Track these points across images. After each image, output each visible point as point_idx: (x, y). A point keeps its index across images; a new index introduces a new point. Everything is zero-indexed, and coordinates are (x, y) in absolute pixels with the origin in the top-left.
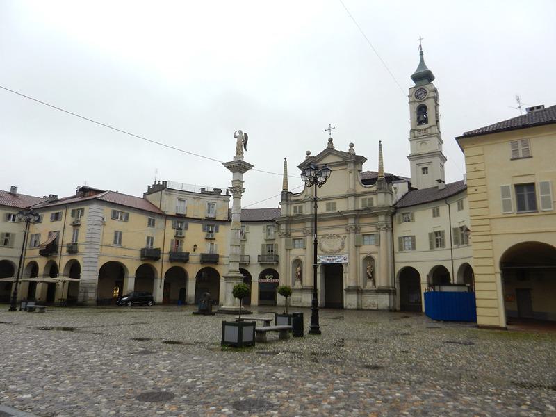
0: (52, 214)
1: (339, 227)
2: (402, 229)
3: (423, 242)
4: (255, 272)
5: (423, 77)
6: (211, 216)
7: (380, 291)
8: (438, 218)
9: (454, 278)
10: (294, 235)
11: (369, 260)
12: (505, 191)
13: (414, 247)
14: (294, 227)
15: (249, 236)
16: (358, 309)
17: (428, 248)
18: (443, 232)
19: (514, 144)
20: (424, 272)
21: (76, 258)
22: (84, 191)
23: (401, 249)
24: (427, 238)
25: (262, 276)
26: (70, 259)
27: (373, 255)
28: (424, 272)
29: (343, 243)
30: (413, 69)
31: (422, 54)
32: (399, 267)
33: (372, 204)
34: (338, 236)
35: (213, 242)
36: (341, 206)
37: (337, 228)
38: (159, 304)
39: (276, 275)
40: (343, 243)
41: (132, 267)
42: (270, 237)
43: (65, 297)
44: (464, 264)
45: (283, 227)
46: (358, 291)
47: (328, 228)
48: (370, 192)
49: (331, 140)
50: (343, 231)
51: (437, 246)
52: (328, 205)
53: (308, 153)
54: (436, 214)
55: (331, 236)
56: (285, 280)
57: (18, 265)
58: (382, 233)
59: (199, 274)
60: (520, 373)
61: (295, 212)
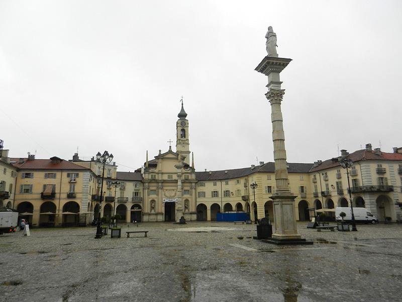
0: (23, 174)
2: (200, 189)
4: (129, 206)
5: (182, 115)
6: (109, 176)
7: (191, 213)
9: (234, 208)
10: (152, 188)
11: (187, 201)
12: (266, 187)
13: (205, 197)
16: (156, 222)
19: (268, 176)
21: (75, 201)
23: (199, 197)
24: (211, 193)
25: (133, 208)
26: (43, 202)
30: (179, 111)
31: (182, 104)
32: (198, 204)
33: (188, 178)
38: (129, 223)
39: (140, 207)
41: (37, 205)
42: (136, 189)
43: (61, 222)
44: (227, 204)
45: (147, 184)
46: (149, 214)
47: (169, 186)
48: (188, 173)
49: (170, 147)
53: (160, 151)
54: (215, 185)
55: (170, 190)
56: (147, 208)
57: (113, 206)
58: (193, 190)
60: (87, 266)
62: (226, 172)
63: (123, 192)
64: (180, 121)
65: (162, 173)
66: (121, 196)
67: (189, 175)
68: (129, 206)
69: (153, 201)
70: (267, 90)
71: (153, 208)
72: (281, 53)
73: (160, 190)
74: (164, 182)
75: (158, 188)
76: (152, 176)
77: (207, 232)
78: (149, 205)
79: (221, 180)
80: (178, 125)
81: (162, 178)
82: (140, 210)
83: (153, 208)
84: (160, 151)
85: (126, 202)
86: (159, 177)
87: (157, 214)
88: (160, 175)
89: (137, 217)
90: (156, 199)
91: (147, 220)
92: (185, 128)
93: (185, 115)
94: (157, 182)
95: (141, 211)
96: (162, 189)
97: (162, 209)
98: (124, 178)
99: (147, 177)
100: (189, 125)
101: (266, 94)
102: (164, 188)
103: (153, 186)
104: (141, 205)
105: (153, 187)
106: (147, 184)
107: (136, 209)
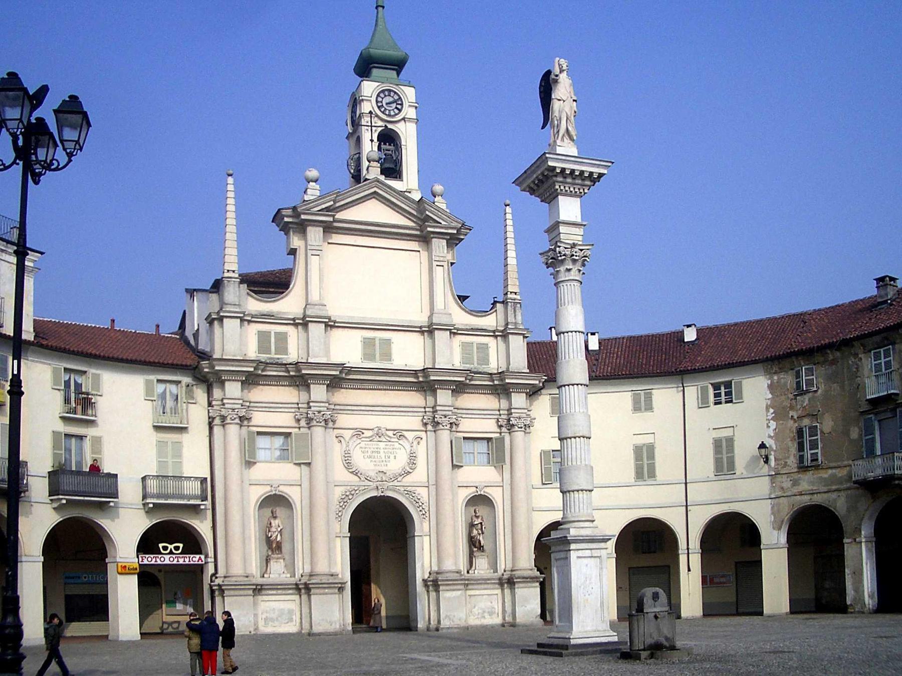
1: (885, 411)
8: (649, 414)
10: (260, 419)
14: (263, 394)
15: (104, 405)
17: (712, 476)
25: (147, 544)
29: (413, 458)
33: (485, 360)
34: (400, 434)
36: (409, 353)
39: (193, 544)
40: (413, 458)
45: (233, 389)
47: (371, 409)
50: (414, 422)
52: (368, 344)
54: (643, 405)
55: (379, 434)
61: (464, 360)
63: (178, 445)
65: (330, 325)
66: (161, 464)
71: (279, 547)
73: (318, 431)
74: (340, 378)
76: (263, 338)
77: (451, 442)
81: (327, 353)
82: (195, 559)
83: (273, 547)
87: (304, 589)
90: (294, 494)
94: (299, 377)
95: (199, 569)
103: (271, 407)
104: (203, 527)
105: (274, 406)
106: (233, 389)
107: (170, 556)
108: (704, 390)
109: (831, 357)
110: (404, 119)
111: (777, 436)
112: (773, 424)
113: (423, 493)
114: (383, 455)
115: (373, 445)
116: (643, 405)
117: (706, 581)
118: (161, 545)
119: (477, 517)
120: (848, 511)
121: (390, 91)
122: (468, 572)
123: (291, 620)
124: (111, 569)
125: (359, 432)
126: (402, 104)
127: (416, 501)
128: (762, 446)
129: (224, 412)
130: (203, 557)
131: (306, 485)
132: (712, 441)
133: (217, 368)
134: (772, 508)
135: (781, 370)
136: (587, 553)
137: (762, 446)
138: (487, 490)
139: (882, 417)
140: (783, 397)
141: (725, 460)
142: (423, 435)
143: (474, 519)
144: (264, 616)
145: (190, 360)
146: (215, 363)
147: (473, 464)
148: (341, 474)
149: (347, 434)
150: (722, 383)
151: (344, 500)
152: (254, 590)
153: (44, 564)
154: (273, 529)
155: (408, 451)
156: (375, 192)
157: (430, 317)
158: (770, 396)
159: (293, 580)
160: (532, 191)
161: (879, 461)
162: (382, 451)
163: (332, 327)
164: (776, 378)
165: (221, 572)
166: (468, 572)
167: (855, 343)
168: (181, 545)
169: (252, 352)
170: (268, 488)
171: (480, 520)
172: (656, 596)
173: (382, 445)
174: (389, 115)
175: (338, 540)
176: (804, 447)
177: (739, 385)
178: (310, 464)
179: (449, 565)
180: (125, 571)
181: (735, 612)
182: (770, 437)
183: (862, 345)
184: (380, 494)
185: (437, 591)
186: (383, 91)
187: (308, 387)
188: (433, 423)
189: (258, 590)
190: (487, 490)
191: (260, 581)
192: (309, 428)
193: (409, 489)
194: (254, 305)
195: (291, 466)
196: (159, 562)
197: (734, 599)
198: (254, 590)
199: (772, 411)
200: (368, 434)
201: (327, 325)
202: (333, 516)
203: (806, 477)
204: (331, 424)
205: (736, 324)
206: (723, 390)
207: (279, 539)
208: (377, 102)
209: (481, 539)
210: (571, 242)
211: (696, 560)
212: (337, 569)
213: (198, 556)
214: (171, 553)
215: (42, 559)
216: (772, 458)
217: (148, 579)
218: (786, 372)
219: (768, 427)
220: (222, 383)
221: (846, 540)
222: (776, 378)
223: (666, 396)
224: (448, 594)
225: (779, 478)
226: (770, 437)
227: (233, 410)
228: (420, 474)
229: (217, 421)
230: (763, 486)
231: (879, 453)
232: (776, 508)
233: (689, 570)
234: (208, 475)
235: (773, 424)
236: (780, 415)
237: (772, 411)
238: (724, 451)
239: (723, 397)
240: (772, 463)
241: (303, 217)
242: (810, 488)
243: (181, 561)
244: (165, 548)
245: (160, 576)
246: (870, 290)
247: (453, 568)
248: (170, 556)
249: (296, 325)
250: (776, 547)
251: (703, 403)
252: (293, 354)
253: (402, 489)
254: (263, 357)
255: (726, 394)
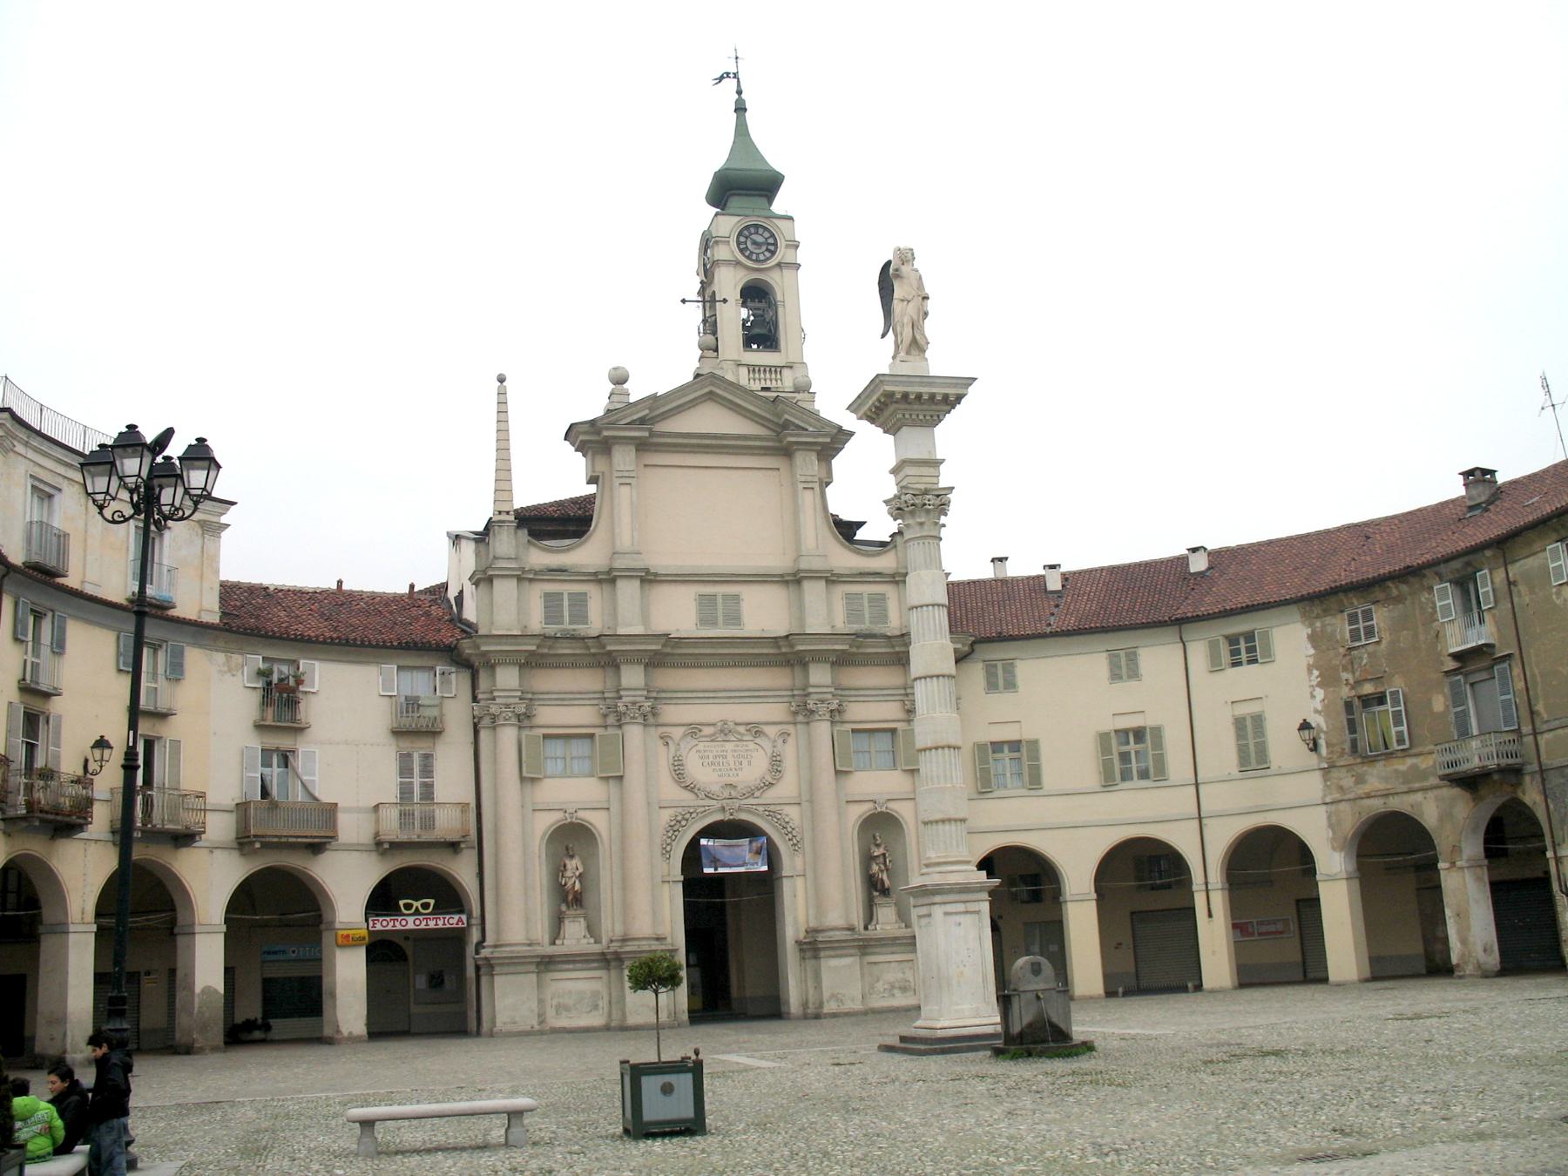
1: (1479, 670)
3: (1070, 760)
4: (347, 884)
5: (744, 187)
8: (1134, 684)
10: (549, 716)
13: (1035, 780)
16: (607, 1028)
17: (1235, 773)
18: (1157, 731)
20: (1205, 857)
22: (926, 314)
25: (382, 899)
27: (895, 807)
28: (1205, 857)
29: (776, 764)
30: (716, 156)
31: (740, 109)
33: (883, 617)
34: (756, 729)
35: (407, 722)
36: (764, 614)
37: (757, 701)
39: (448, 896)
45: (507, 678)
50: (772, 711)
51: (1126, 776)
52: (706, 602)
53: (619, 379)
55: (724, 731)
56: (516, 910)
59: (244, 900)
62: (1198, 564)
64: (729, 225)
65: (649, 578)
67: (889, 590)
68: (347, 884)
69: (572, 837)
70: (891, 490)
71: (577, 900)
72: (940, 362)
74: (664, 653)
75: (615, 715)
76: (552, 601)
78: (540, 875)
79: (1180, 623)
80: (721, 253)
81: (645, 618)
82: (453, 921)
83: (570, 899)
84: (619, 379)
85: (316, 848)
86: (629, 614)
88: (628, 590)
89: (430, 985)
91: (529, 1021)
92: (774, 279)
93: (766, 185)
94: (603, 655)
95: (456, 939)
96: (649, 718)
97: (660, 918)
98: (282, 630)
99: (507, 612)
100: (801, 256)
101: (886, 502)
102: (671, 713)
104: (462, 871)
105: (569, 700)
106: (507, 678)
107: (412, 919)
108: (1213, 646)
109: (1395, 592)
110: (779, 265)
111: (1326, 711)
112: (1320, 693)
113: (793, 813)
114: (730, 759)
115: (715, 748)
116: (1124, 669)
117: (1239, 927)
118: (401, 903)
119: (878, 846)
120: (1441, 819)
121: (757, 226)
122: (866, 928)
123: (596, 1007)
124: (327, 938)
125: (694, 730)
126: (775, 244)
127: (784, 826)
128: (1305, 726)
129: (493, 709)
130: (464, 917)
131: (615, 808)
132: (1231, 720)
133: (484, 648)
134: (1329, 818)
135: (1326, 612)
136: (961, 907)
137: (1305, 726)
138: (892, 805)
139: (1472, 679)
140: (1331, 653)
141: (1252, 748)
142: (791, 729)
143: (873, 848)
144: (554, 1002)
145: (447, 636)
146: (479, 641)
147: (869, 767)
148: (671, 792)
149: (677, 733)
150: (1242, 634)
151: (674, 828)
152: (538, 964)
153: (227, 936)
154: (568, 874)
155: (769, 751)
156: (711, 392)
157: (796, 560)
158: (1312, 651)
159: (597, 948)
160: (872, 420)
161: (1474, 744)
162: (729, 755)
163: (651, 581)
164: (1318, 624)
165: (489, 941)
166: (866, 928)
167: (1426, 572)
168: (432, 902)
169: (536, 623)
170: (560, 815)
171: (882, 850)
172: (1036, 969)
173: (729, 746)
174: (757, 261)
175: (666, 886)
176: (1359, 725)
177: (1266, 636)
178: (621, 778)
179: (834, 918)
180: (349, 942)
181: (1301, 977)
182: (1316, 711)
183: (1436, 573)
184: (727, 817)
185: (816, 957)
186: (747, 228)
187: (617, 667)
188: (803, 712)
189: (546, 963)
190: (892, 805)
191: (550, 950)
192: (620, 726)
193: (772, 808)
194: (539, 557)
195: (593, 781)
196: (399, 927)
197: (1298, 957)
198: (538, 964)
199: (1316, 673)
200: (707, 731)
201: (643, 581)
202: (658, 850)
203: (1375, 771)
204: (651, 720)
205: (1270, 543)
206: (1243, 646)
207: (577, 887)
208: (738, 243)
209: (885, 877)
210: (922, 487)
211: (1219, 900)
212: (664, 930)
213: (456, 917)
214: (417, 912)
215: (224, 928)
216: (1322, 742)
217: (382, 952)
218: (1333, 615)
219: (1313, 697)
220: (492, 667)
221: (1441, 865)
222: (1318, 624)
223: (1159, 658)
224: (834, 962)
225: (1335, 773)
226: (1316, 711)
227: (507, 706)
228: (787, 788)
229: (486, 721)
230: (1313, 786)
231: (1475, 732)
232: (1334, 819)
233: (1210, 915)
234: (471, 799)
235: (1320, 693)
236: (1328, 679)
237: (1316, 673)
238: (1250, 735)
239: (1244, 656)
240: (1324, 750)
241: (606, 433)
242: (1382, 786)
243: (432, 924)
244: (408, 907)
245: (408, 948)
246: (1457, 489)
247: (841, 923)
248: (412, 919)
249: (600, 581)
250: (1332, 878)
251: (1215, 666)
252: (595, 623)
253: (761, 808)
254: (552, 629)
255: (1246, 650)
